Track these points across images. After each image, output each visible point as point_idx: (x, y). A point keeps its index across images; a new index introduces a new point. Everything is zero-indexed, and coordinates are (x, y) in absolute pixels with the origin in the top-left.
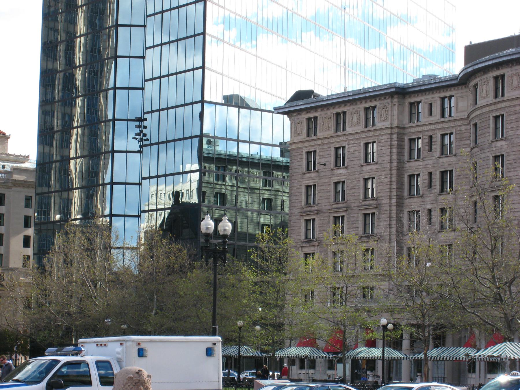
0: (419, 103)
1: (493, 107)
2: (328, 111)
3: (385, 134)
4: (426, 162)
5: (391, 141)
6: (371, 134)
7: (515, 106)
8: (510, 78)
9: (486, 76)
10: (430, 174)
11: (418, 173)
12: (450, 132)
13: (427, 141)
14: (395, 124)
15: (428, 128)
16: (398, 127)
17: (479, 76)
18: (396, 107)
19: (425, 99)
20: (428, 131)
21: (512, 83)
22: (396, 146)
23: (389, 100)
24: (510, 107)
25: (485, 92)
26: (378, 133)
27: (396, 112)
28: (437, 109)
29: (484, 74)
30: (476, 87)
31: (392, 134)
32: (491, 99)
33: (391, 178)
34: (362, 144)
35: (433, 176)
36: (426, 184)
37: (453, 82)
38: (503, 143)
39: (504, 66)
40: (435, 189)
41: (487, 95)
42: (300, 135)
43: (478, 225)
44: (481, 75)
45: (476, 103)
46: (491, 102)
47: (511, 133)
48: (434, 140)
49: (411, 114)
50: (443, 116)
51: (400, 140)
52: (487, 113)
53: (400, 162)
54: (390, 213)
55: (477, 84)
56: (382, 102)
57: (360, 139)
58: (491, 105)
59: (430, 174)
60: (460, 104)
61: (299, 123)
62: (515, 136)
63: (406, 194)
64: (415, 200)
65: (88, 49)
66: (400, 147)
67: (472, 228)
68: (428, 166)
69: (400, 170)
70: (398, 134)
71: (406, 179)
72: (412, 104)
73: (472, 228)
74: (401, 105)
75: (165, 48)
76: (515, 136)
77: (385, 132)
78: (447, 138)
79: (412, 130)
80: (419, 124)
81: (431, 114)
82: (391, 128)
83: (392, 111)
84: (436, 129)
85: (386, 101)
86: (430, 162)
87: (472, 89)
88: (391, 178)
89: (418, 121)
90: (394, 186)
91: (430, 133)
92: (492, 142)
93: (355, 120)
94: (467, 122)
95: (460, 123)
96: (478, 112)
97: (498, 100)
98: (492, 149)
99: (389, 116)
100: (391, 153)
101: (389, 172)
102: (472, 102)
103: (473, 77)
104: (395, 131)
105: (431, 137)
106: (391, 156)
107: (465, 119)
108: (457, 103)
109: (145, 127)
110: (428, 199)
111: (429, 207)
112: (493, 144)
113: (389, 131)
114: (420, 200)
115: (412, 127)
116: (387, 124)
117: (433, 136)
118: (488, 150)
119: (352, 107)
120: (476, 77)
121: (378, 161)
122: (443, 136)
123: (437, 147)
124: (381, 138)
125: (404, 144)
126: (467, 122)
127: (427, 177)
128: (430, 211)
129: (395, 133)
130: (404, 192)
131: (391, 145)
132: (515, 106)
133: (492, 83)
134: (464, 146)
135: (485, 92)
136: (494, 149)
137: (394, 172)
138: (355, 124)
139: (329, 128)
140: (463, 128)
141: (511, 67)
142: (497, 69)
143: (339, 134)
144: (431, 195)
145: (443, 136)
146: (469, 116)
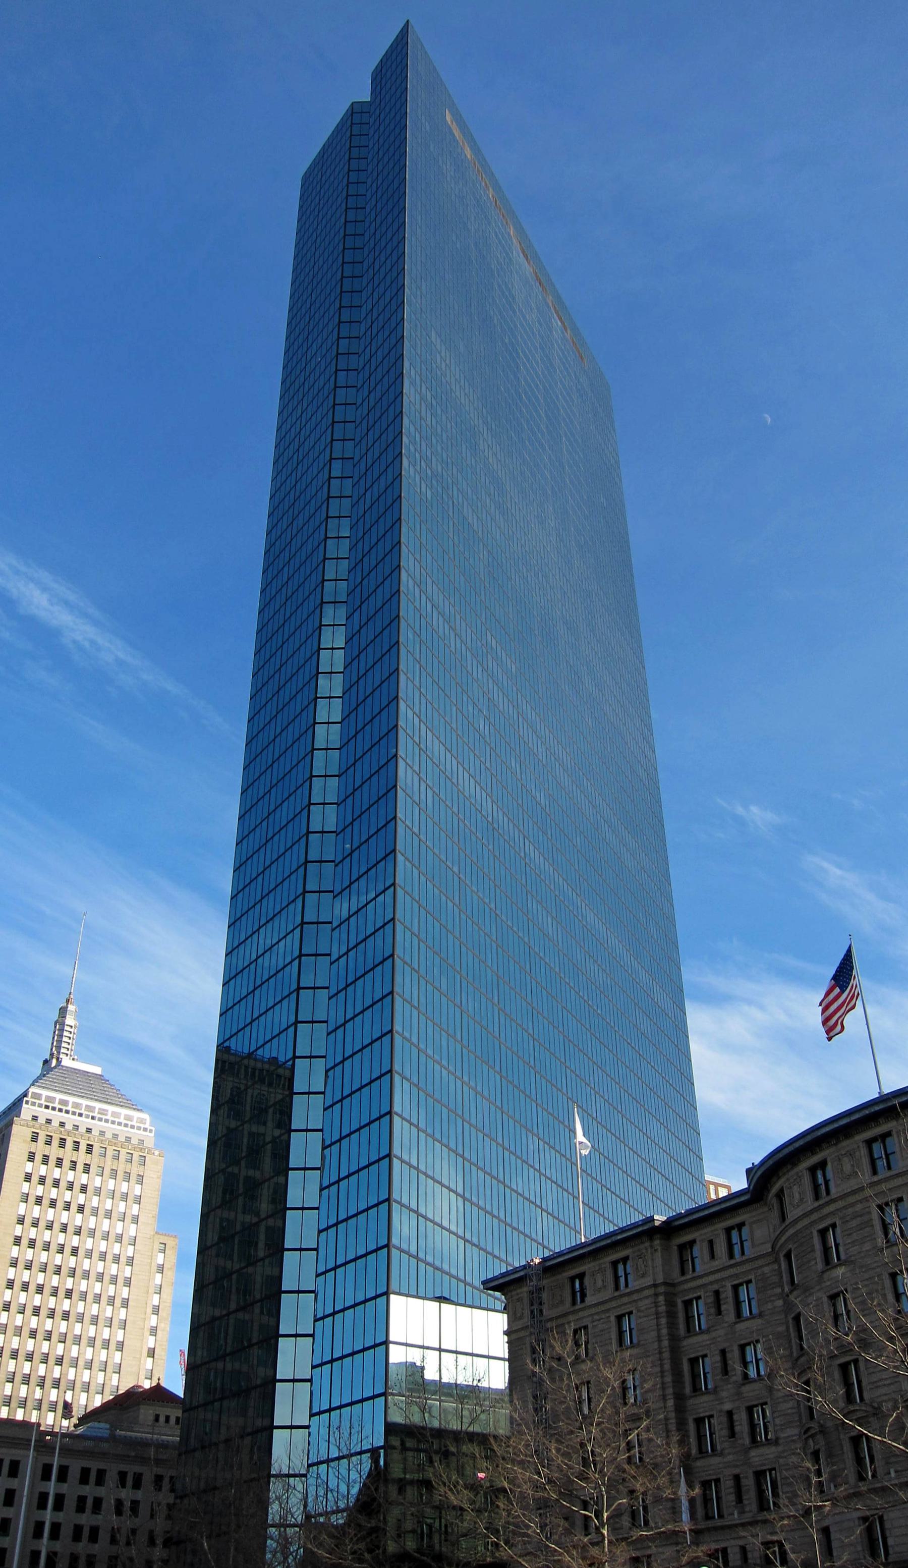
0: (692, 1243)
1: (815, 1216)
2: (559, 1277)
3: (647, 1297)
4: (714, 1334)
5: (656, 1306)
6: (625, 1300)
7: (852, 1205)
8: (835, 1163)
9: (796, 1170)
10: (723, 1352)
11: (705, 1352)
12: (746, 1279)
13: (711, 1300)
14: (660, 1280)
15: (711, 1278)
16: (665, 1284)
17: (784, 1174)
18: (659, 1254)
19: (700, 1235)
20: (711, 1283)
21: (842, 1170)
22: (664, 1314)
23: (647, 1244)
24: (845, 1208)
25: (797, 1196)
26: (635, 1297)
27: (659, 1261)
28: (721, 1248)
29: (792, 1168)
30: (780, 1195)
31: (656, 1295)
32: (810, 1203)
33: (662, 1365)
34: (613, 1319)
35: (728, 1355)
36: (719, 1370)
37: (743, 1199)
38: (840, 1271)
39: (824, 1145)
40: (735, 1375)
41: (801, 1200)
42: (521, 1318)
43: (819, 1423)
44: (788, 1171)
45: (783, 1218)
46: (809, 1209)
47: (854, 1250)
48: (722, 1296)
49: (682, 1263)
50: (731, 1255)
51: (671, 1304)
52: (806, 1227)
53: (674, 1339)
54: (666, 1425)
55: (782, 1190)
56: (636, 1248)
57: (608, 1310)
58: (811, 1212)
59: (723, 1352)
60: (759, 1232)
61: (518, 1300)
62: (862, 1254)
63: (688, 1390)
64: (705, 1398)
65: (72, 597)
66: (671, 1315)
67: (808, 1429)
68: (719, 1339)
69: (675, 1350)
70: (666, 1294)
71: (686, 1367)
72: (682, 1248)
73: (808, 1429)
74: (666, 1249)
75: (340, 1271)
76: (862, 1254)
77: (647, 1293)
78: (743, 1290)
79: (686, 1286)
80: (696, 1274)
81: (713, 1256)
82: (655, 1286)
83: (653, 1260)
84: (723, 1279)
85: (642, 1246)
86: (721, 1332)
87: (775, 1201)
88: (662, 1365)
89: (694, 1270)
90: (668, 1379)
91: (716, 1287)
92: (823, 1272)
93: (599, 1283)
94: (771, 1259)
95: (760, 1262)
96: (791, 1231)
97: (821, 1202)
98: (824, 1285)
99: (651, 1267)
100: (658, 1325)
101: (658, 1356)
102: (777, 1221)
103: (774, 1179)
104: (662, 1289)
105: (717, 1293)
106: (659, 1330)
107: (768, 1254)
108: (752, 1232)
109: (128, 1139)
110: (724, 1394)
111: (727, 1407)
112: (826, 1276)
113: (651, 1292)
114: (711, 1397)
115: (686, 1281)
116: (648, 1281)
117: (721, 1290)
118: (818, 1288)
119: (592, 1264)
120: (779, 1178)
121: (639, 1341)
122: (736, 1288)
123: (728, 1307)
124: (640, 1304)
125: (676, 1310)
126: (771, 1259)
127: (718, 1358)
128: (730, 1414)
129: (661, 1294)
130: (684, 1388)
131: (657, 1313)
132: (852, 1205)
133: (807, 1179)
134: (772, 1298)
135: (797, 1196)
136: (828, 1283)
137: (666, 1355)
138: (598, 1279)
139: (562, 1302)
140: (766, 1270)
141: (836, 1144)
142: (813, 1154)
143: (577, 1307)
144: (729, 1386)
145: (736, 1288)
146: (773, 1248)
